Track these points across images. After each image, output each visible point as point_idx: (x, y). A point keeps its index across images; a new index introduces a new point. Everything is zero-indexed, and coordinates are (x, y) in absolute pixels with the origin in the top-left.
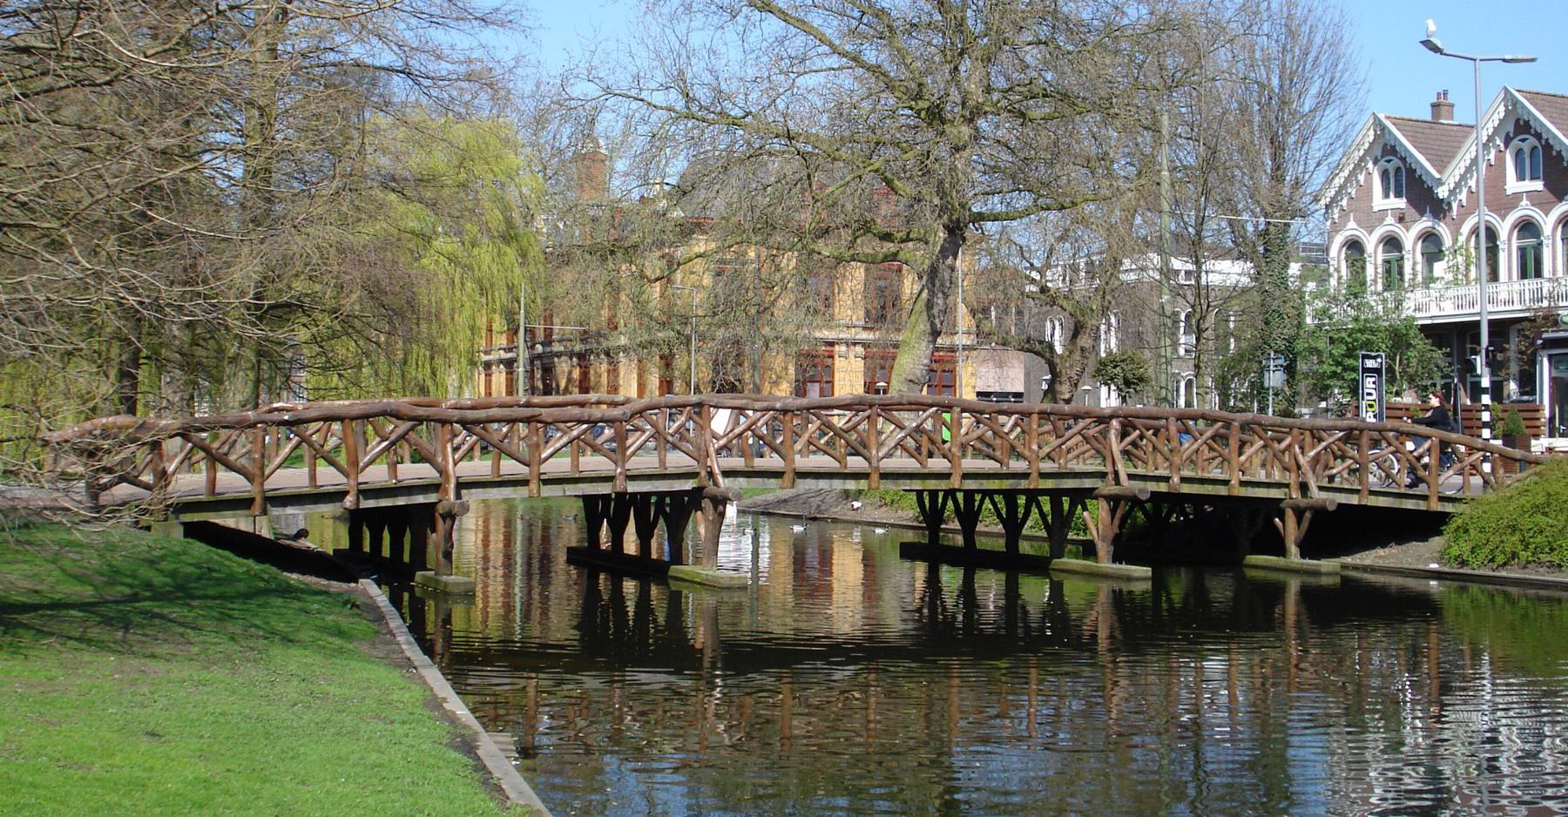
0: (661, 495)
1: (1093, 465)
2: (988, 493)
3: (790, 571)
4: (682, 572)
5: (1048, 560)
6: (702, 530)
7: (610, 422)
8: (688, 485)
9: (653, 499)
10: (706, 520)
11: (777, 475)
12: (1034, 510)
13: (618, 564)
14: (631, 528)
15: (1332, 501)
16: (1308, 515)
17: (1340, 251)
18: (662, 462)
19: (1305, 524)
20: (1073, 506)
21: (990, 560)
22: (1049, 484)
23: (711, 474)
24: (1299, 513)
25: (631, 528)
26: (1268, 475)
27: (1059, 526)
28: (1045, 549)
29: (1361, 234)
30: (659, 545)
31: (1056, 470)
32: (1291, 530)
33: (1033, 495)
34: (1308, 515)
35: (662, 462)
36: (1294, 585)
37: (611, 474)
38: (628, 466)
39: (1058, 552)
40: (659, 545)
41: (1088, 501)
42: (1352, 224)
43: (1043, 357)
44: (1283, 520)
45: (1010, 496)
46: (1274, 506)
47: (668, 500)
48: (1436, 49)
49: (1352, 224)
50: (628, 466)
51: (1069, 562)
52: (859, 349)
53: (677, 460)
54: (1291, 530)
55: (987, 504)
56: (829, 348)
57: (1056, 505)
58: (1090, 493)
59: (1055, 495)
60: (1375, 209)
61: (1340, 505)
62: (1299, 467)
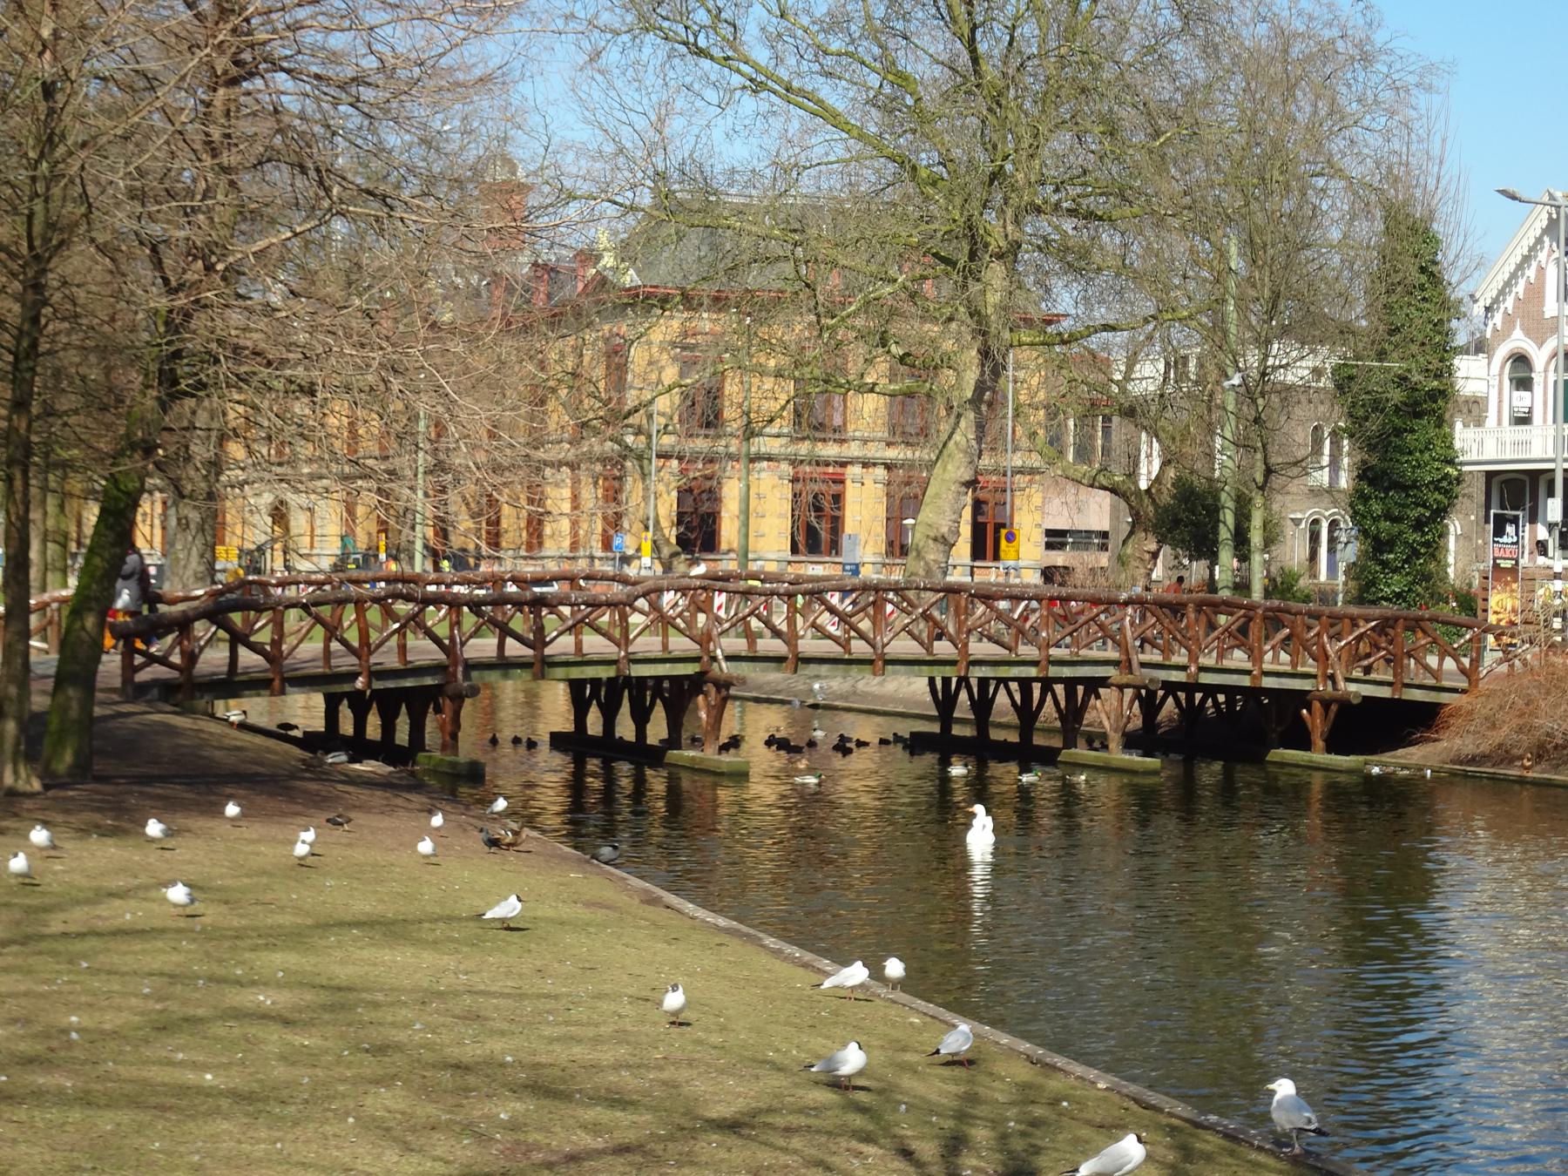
0: (659, 679)
1: (1112, 654)
2: (1003, 681)
3: (557, 1103)
4: (682, 757)
5: (1057, 751)
6: (703, 715)
7: (610, 604)
8: (690, 669)
9: (650, 683)
10: (708, 705)
11: (780, 660)
12: (1049, 697)
13: (609, 747)
14: (625, 708)
15: (1356, 694)
16: (1334, 708)
17: (1503, 367)
18: (665, 646)
19: (1332, 715)
20: (1087, 695)
21: (1004, 752)
22: (1067, 672)
23: (714, 659)
24: (1326, 704)
25: (625, 708)
26: (1294, 664)
27: (1072, 715)
28: (1056, 742)
29: (1529, 347)
30: (657, 730)
31: (1068, 658)
32: (1316, 722)
33: (1047, 684)
34: (1334, 708)
35: (665, 646)
36: (1318, 780)
37: (615, 657)
38: (631, 650)
39: (1070, 743)
40: (657, 730)
41: (1101, 690)
42: (1518, 333)
43: (1127, 500)
44: (1309, 711)
45: (1025, 684)
46: (1302, 698)
47: (666, 684)
48: (1513, 197)
49: (1518, 333)
50: (631, 650)
51: (1081, 752)
52: (880, 472)
53: (680, 644)
54: (1316, 722)
55: (1002, 691)
56: (839, 470)
57: (1190, 699)
58: (1103, 682)
59: (1070, 683)
60: (1547, 316)
61: (1365, 698)
62: (1327, 657)
